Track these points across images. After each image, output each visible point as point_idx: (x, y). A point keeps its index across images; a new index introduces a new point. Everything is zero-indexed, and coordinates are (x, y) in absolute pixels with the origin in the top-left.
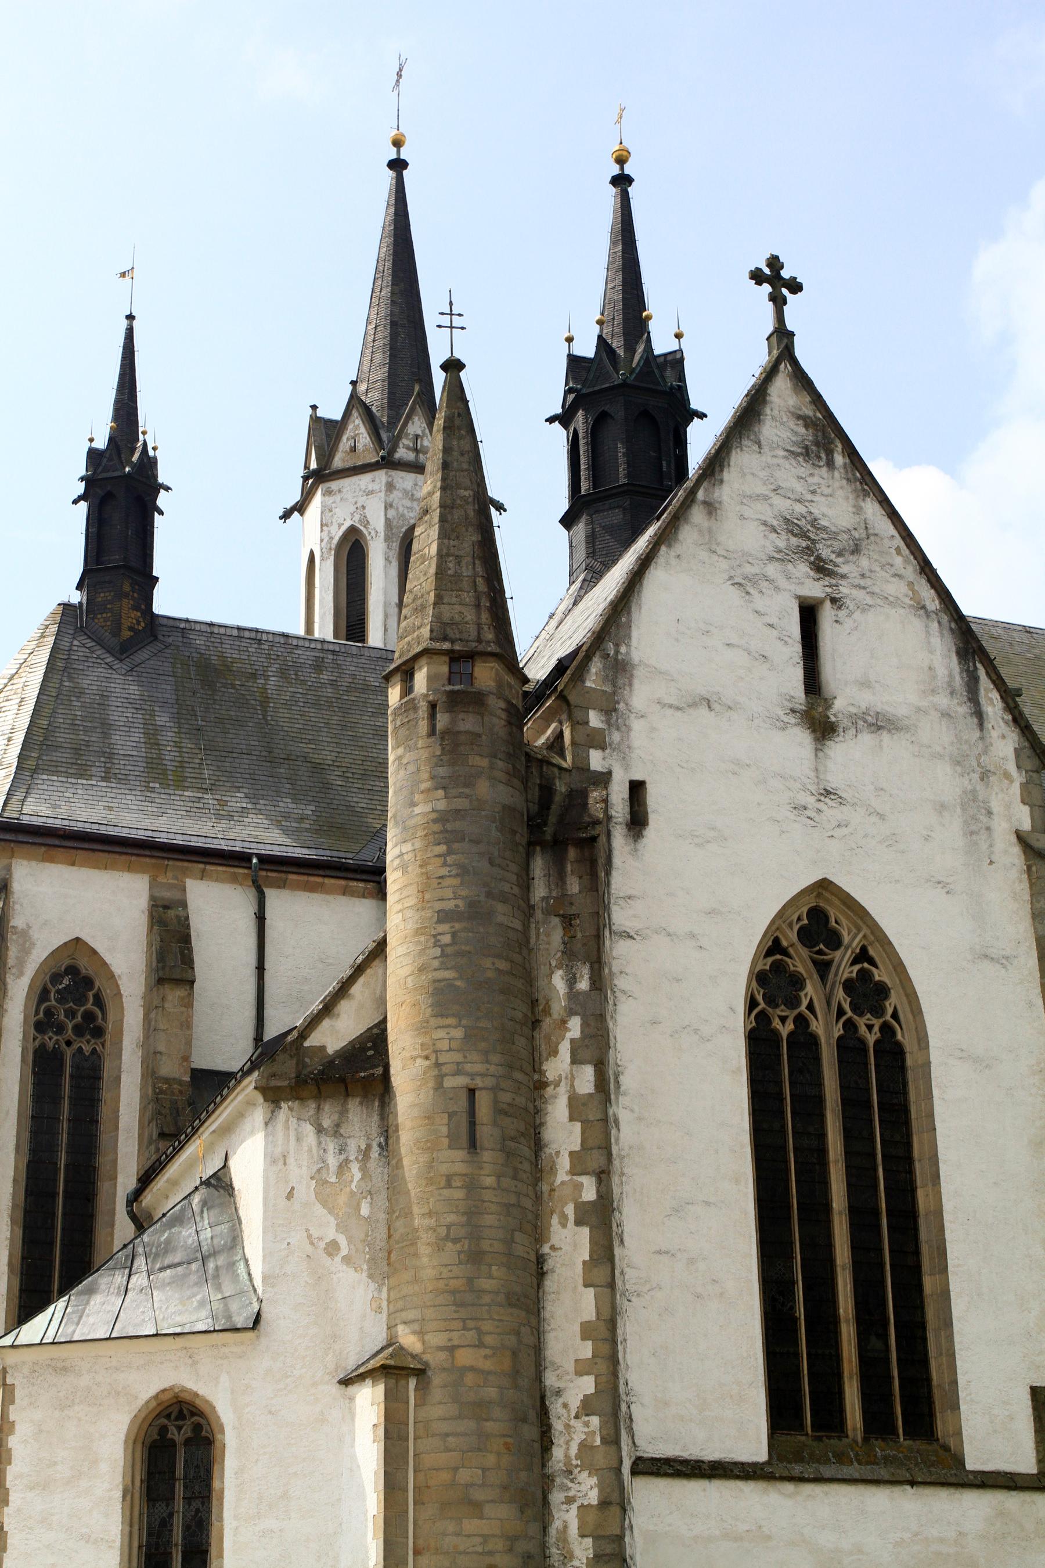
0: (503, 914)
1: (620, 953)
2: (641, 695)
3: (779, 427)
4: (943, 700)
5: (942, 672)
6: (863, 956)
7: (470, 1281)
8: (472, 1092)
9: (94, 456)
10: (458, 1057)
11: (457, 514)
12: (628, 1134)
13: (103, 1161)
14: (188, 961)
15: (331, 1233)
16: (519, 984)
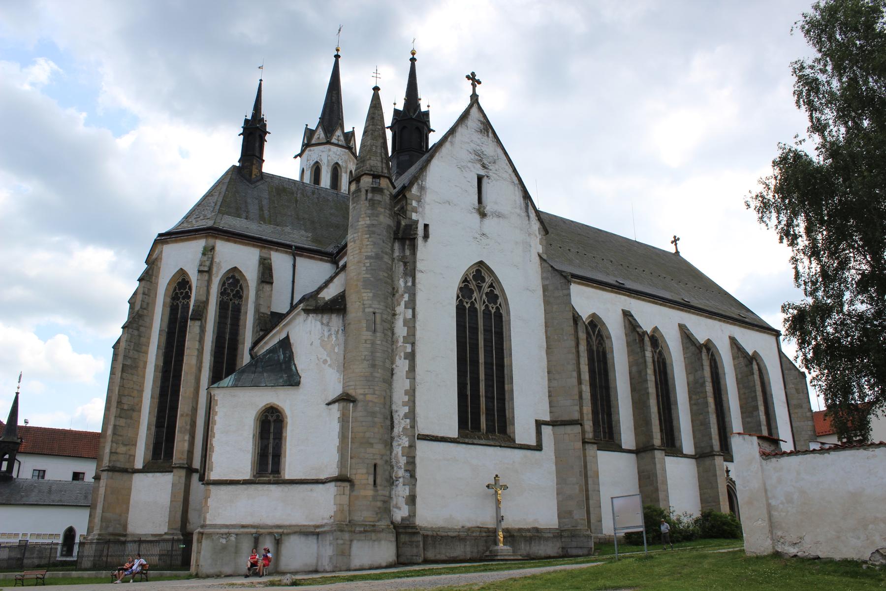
0: (386, 259)
1: (419, 275)
2: (428, 197)
3: (474, 121)
4: (518, 211)
5: (518, 202)
6: (491, 286)
7: (372, 373)
9: (246, 121)
10: (370, 302)
11: (376, 133)
12: (419, 334)
13: (240, 338)
14: (271, 276)
15: (325, 357)
16: (390, 281)
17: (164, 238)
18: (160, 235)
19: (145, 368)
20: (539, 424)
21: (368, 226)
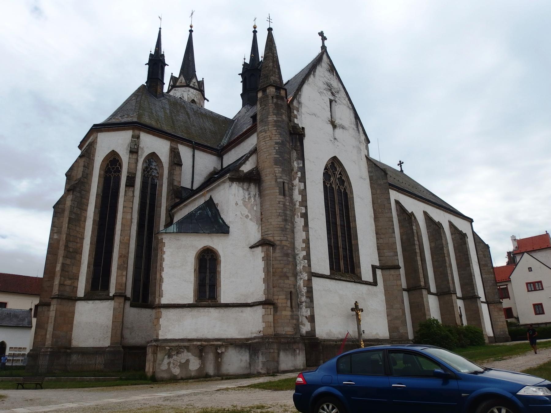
2: (303, 110)
6: (340, 174)
8: (284, 183)
9: (151, 55)
15: (247, 213)
17: (97, 129)
18: (95, 125)
19: (85, 221)
20: (374, 268)
21: (275, 121)
